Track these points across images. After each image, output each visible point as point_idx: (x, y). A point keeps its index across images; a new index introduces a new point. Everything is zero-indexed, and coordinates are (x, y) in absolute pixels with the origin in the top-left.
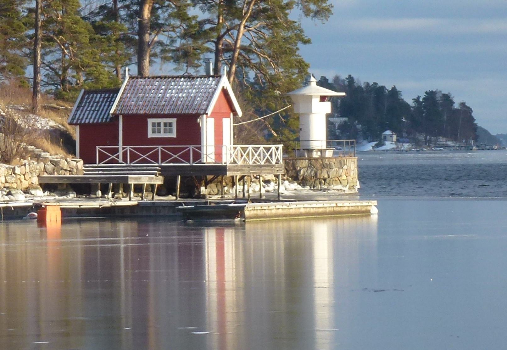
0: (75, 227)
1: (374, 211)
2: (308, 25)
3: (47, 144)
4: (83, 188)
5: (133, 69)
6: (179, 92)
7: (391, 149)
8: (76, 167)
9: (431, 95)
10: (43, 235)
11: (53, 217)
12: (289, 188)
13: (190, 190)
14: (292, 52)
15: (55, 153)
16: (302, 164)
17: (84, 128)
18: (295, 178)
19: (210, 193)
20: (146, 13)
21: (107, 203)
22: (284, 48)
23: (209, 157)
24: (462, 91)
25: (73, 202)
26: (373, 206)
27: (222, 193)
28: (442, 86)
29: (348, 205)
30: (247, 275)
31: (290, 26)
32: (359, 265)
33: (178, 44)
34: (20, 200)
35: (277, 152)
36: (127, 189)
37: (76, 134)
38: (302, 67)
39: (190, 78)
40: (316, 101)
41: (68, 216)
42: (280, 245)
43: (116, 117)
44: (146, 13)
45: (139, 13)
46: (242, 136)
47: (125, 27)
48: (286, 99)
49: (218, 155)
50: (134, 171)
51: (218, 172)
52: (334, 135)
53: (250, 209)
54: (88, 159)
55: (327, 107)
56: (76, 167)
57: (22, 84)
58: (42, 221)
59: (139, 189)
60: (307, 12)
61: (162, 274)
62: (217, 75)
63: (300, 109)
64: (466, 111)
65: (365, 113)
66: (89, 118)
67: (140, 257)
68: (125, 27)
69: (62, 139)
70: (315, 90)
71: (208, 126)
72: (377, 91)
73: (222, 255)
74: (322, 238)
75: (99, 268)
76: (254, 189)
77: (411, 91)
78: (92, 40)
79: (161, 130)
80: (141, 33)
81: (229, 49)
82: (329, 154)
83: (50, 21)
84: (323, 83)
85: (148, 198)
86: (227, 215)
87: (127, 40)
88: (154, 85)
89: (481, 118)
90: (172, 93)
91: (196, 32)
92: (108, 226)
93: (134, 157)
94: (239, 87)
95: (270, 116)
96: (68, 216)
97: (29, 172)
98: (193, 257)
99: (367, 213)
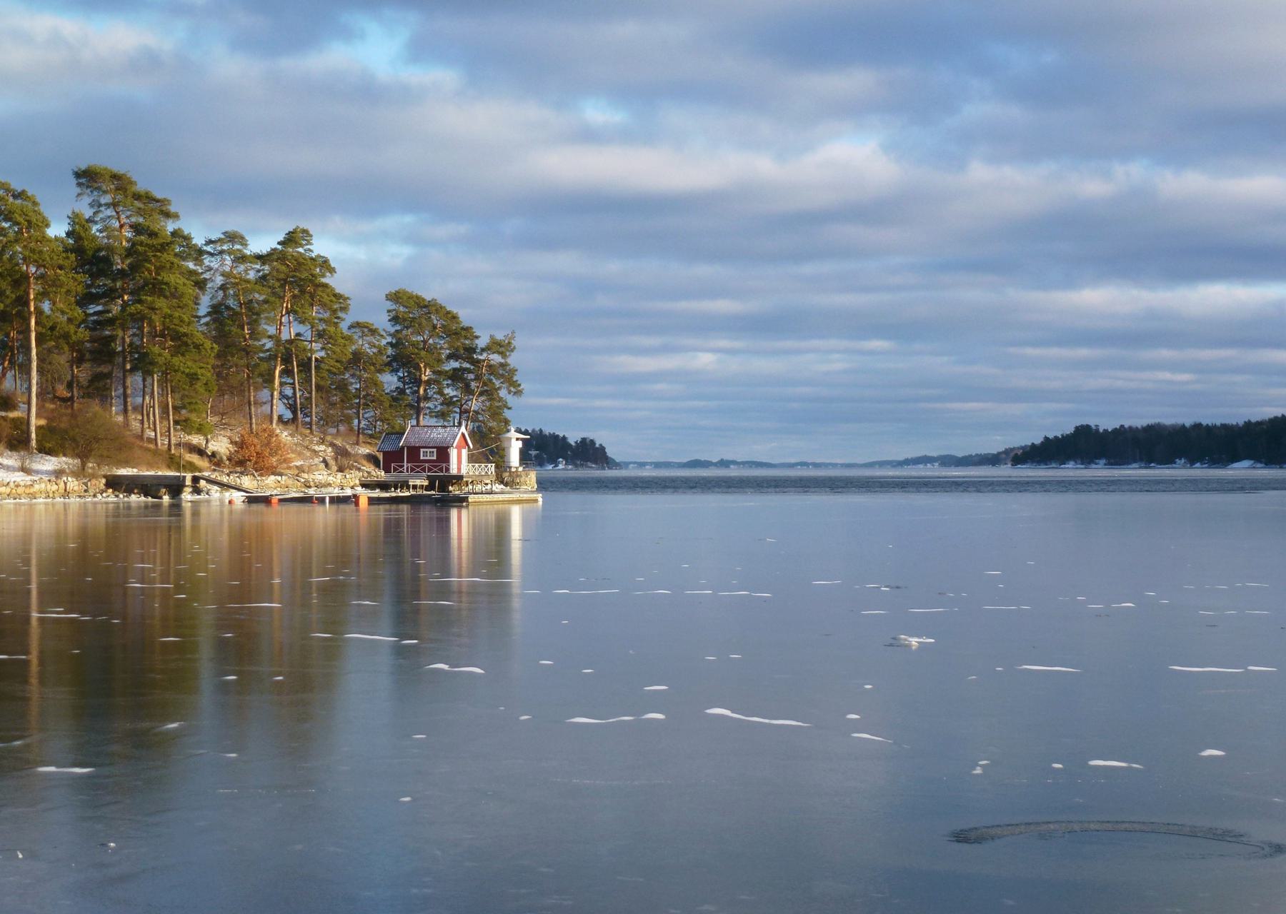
0: (372, 507)
1: (540, 500)
2: (511, 399)
3: (365, 462)
4: (384, 486)
5: (414, 422)
6: (438, 434)
7: (562, 469)
8: (381, 475)
9: (584, 440)
10: (357, 511)
11: (363, 502)
12: (498, 487)
13: (443, 488)
14: (500, 414)
15: (369, 468)
16: (506, 475)
17: (385, 453)
18: (502, 482)
19: (454, 490)
20: (422, 391)
21: (394, 494)
22: (497, 411)
23: (454, 470)
24: (601, 437)
25: (377, 493)
26: (539, 497)
27: (460, 490)
28: (590, 435)
29: (525, 496)
30: (474, 533)
31: (500, 399)
32: (540, 529)
33: (439, 408)
34: (349, 492)
35: (492, 468)
36: (408, 487)
37: (381, 457)
38: (507, 422)
39: (445, 427)
40: (513, 441)
41: (372, 501)
42: (492, 518)
43: (403, 448)
44: (422, 391)
45: (418, 392)
46: (472, 459)
47: (410, 399)
48: (498, 439)
49: (459, 469)
50: (412, 477)
51: (458, 479)
52: (525, 457)
53: (471, 498)
54: (387, 470)
55: (520, 444)
56: (381, 475)
57: (351, 430)
58: (357, 504)
59: (415, 487)
60: (510, 392)
61: (427, 535)
62: (460, 424)
63: (505, 444)
64: (602, 449)
65: (543, 448)
66: (388, 447)
67: (415, 522)
68: (410, 399)
69: (372, 459)
70: (513, 434)
71: (453, 453)
72: (555, 437)
73: (461, 524)
74: (516, 513)
75: (392, 527)
76: (478, 488)
77: (573, 438)
78: (391, 406)
79: (428, 455)
80: (418, 402)
81: (467, 411)
82: (521, 469)
83: (368, 395)
84: (519, 431)
85: (420, 492)
86: (461, 501)
87: (411, 406)
88: (424, 431)
89: (610, 452)
90: (434, 435)
91: (449, 402)
92: (394, 507)
93: (412, 470)
94: (472, 434)
95: (487, 446)
96: (372, 501)
97: (354, 477)
98: (444, 523)
99: (536, 501)
